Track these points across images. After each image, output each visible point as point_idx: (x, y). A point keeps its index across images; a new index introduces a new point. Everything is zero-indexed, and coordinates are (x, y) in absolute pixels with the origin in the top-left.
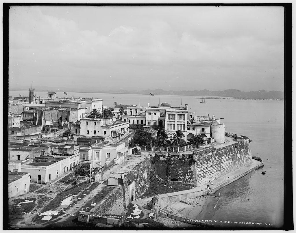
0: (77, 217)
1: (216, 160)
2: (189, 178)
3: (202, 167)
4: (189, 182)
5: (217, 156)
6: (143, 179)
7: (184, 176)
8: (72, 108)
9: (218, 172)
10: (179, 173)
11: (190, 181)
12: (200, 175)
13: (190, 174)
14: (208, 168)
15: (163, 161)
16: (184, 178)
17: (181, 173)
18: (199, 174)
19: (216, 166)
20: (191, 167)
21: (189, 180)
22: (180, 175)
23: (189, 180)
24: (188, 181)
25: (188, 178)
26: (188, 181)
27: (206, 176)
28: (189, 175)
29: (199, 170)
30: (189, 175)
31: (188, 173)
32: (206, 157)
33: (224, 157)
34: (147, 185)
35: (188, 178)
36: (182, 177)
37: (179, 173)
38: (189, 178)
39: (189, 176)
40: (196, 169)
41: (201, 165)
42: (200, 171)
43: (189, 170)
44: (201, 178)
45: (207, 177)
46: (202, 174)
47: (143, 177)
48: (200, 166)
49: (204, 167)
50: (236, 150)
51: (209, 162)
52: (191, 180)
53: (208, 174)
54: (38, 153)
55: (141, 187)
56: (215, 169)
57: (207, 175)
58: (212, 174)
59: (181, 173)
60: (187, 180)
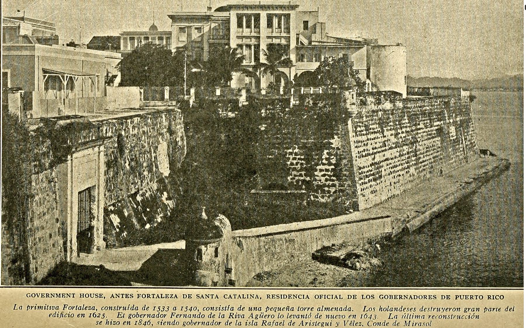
0: (20, 277)
1: (404, 130)
2: (326, 180)
3: (369, 142)
4: (329, 192)
5: (406, 118)
6: (150, 171)
7: (310, 171)
8: (217, 249)
9: (412, 170)
10: (292, 164)
11: (333, 190)
12: (366, 170)
13: (330, 164)
14: (385, 150)
15: (227, 121)
16: (308, 179)
17: (297, 164)
18: (361, 166)
19: (405, 147)
20: (336, 137)
21: (329, 186)
22: (294, 169)
23: (329, 186)
24: (323, 191)
25: (323, 179)
26: (323, 191)
27: (381, 177)
28: (327, 167)
29: (361, 149)
30: (327, 167)
31: (324, 161)
32: (377, 111)
33: (422, 126)
34: (169, 198)
35: (323, 179)
36: (301, 175)
37: (292, 164)
38: (326, 180)
39: (327, 170)
40: (353, 147)
41: (367, 134)
42: (364, 154)
43: (326, 152)
44: (369, 181)
45: (382, 179)
46: (370, 168)
47: (152, 165)
48: (364, 138)
49: (374, 146)
50: (446, 115)
51: (387, 130)
52: (334, 185)
53: (388, 171)
54: (55, 175)
55: (139, 198)
56: (403, 158)
57: (383, 173)
58: (398, 173)
59: (297, 164)
60: (321, 187)
